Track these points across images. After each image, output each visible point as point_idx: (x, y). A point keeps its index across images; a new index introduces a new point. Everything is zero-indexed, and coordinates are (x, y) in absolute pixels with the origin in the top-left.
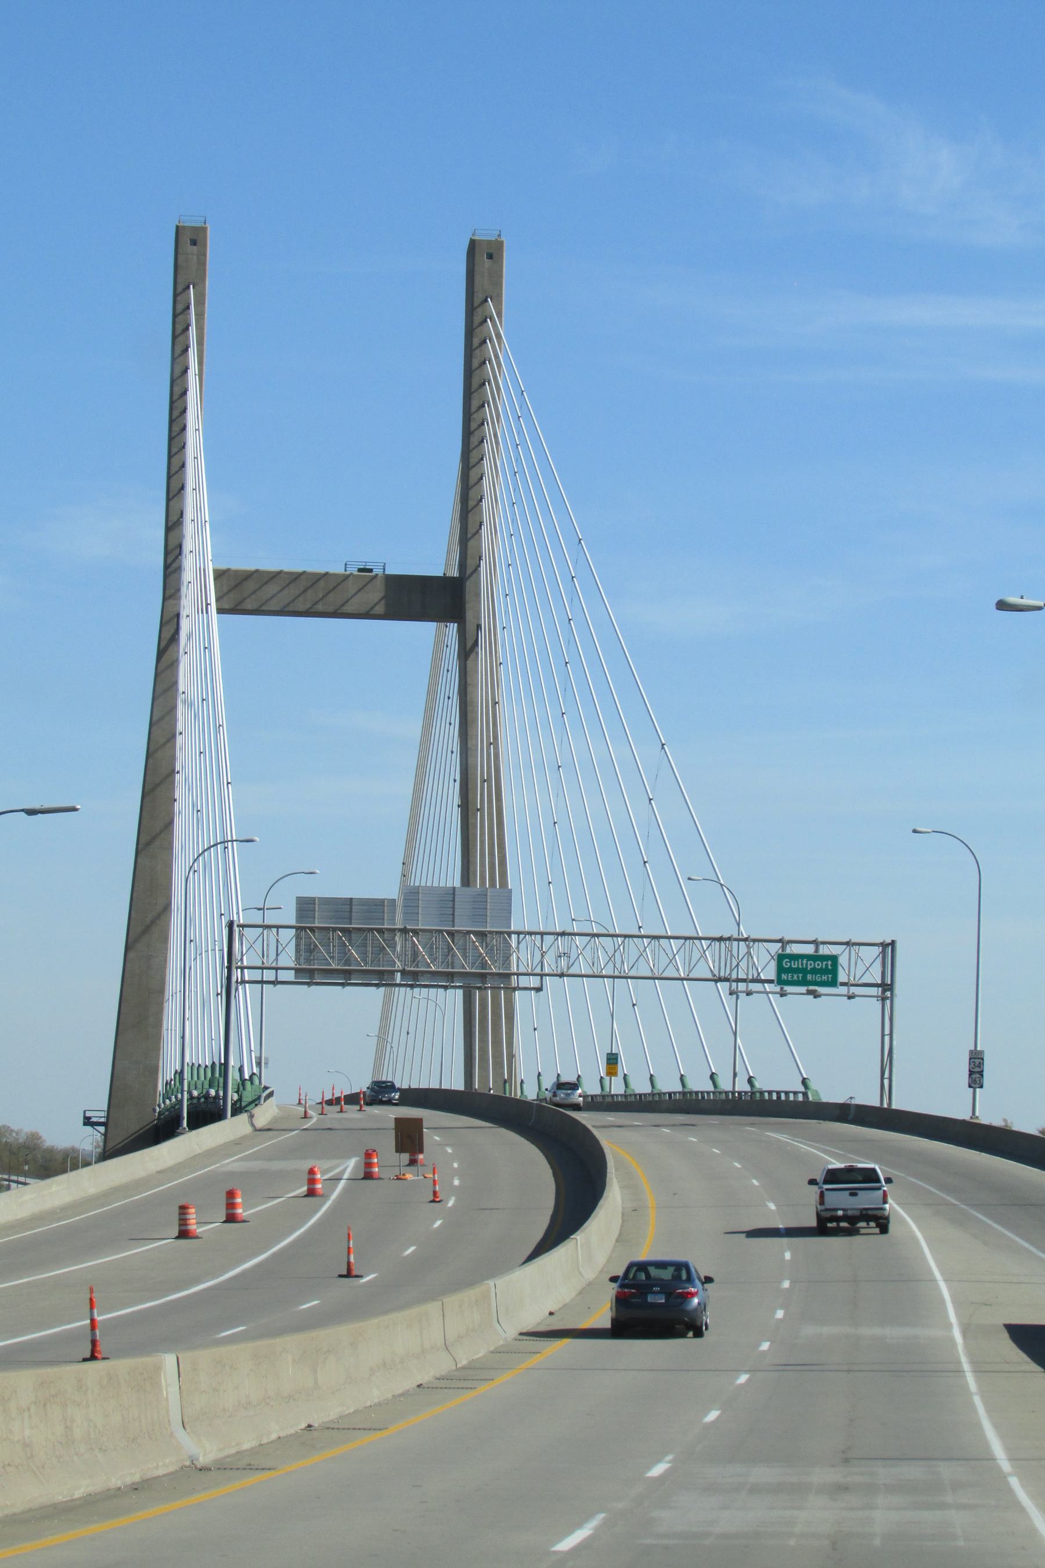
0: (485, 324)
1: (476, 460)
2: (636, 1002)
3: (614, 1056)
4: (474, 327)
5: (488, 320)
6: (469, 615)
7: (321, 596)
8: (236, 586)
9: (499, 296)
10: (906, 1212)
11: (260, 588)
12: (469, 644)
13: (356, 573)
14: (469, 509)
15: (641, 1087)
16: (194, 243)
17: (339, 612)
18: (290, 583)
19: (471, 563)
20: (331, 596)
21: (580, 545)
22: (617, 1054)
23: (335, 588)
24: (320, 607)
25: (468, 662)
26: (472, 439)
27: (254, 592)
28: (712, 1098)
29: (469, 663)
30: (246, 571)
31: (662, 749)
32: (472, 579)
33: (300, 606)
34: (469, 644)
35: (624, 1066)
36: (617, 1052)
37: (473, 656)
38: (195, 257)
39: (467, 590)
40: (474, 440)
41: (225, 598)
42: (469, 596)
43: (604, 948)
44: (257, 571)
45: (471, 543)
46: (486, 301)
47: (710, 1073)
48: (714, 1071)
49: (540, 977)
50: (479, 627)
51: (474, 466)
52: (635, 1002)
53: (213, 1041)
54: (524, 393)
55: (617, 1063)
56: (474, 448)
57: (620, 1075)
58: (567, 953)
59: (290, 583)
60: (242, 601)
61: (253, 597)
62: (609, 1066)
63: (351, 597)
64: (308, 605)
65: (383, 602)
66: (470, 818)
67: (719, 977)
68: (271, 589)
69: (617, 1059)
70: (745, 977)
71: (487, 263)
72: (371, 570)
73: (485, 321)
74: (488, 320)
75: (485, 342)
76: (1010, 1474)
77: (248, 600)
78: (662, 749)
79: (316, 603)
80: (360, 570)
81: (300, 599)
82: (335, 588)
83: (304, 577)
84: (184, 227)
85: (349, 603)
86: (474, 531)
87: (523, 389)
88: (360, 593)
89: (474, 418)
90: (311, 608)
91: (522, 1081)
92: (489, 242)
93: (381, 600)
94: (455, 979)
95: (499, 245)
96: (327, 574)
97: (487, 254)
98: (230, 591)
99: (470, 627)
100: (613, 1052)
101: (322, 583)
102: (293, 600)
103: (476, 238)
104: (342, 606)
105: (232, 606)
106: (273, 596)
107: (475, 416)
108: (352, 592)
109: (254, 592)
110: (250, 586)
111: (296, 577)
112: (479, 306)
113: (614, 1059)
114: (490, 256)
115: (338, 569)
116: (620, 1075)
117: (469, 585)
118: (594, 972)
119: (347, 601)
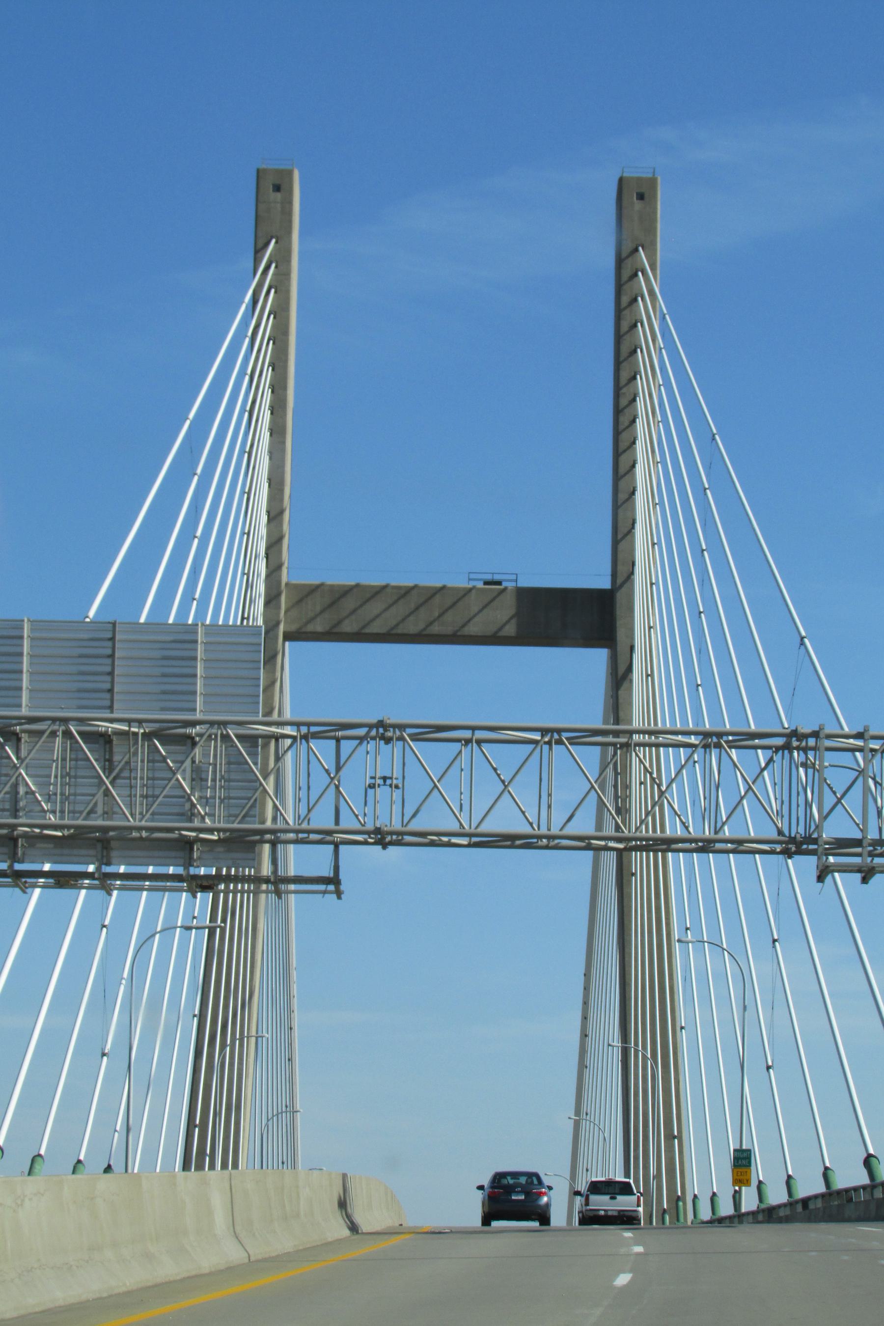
0: (635, 279)
1: (627, 444)
2: (773, 1062)
3: (745, 1155)
4: (622, 283)
5: (640, 274)
6: (621, 634)
7: (437, 614)
8: (332, 604)
9: (653, 243)
10: (237, 740)
11: (361, 606)
12: (622, 670)
13: (480, 585)
14: (619, 504)
15: (777, 1196)
16: (277, 188)
17: (459, 633)
18: (399, 599)
19: (622, 570)
20: (449, 617)
21: (802, 647)
22: (749, 1151)
23: (454, 604)
24: (436, 629)
25: (620, 692)
26: (621, 419)
27: (354, 611)
28: (233, 873)
29: (621, 692)
30: (344, 586)
31: (802, 644)
32: (624, 589)
33: (412, 627)
34: (622, 670)
35: (759, 1169)
36: (749, 1147)
37: (625, 685)
38: (279, 206)
39: (618, 605)
40: (624, 420)
41: (318, 619)
42: (619, 612)
43: (495, 770)
44: (357, 586)
45: (621, 546)
46: (636, 250)
47: (865, 1155)
48: (871, 1151)
49: (332, 847)
50: (632, 648)
51: (625, 451)
52: (770, 1063)
53: (116, 1134)
54: (806, 641)
55: (749, 1165)
56: (624, 430)
57: (754, 1183)
58: (391, 778)
59: (399, 599)
60: (340, 622)
61: (353, 617)
62: (736, 1170)
63: (475, 616)
64: (421, 626)
65: (514, 621)
66: (624, 887)
67: (790, 837)
68: (375, 607)
69: (748, 1158)
70: (858, 835)
71: (638, 205)
72: (499, 583)
73: (636, 275)
74: (640, 274)
75: (635, 300)
76: (808, 846)
77: (346, 622)
78: (802, 644)
79: (431, 623)
80: (486, 583)
81: (411, 618)
82: (454, 604)
83: (414, 592)
84: (265, 170)
85: (472, 622)
86: (626, 530)
87: (803, 634)
88: (485, 611)
89: (624, 394)
90: (425, 629)
91: (695, 1196)
92: (639, 180)
93: (511, 618)
94: (114, 854)
95: (652, 183)
96: (444, 588)
97: (637, 194)
98: (322, 611)
99: (622, 646)
100: (744, 1147)
101: (437, 599)
102: (404, 620)
103: (625, 175)
104: (463, 626)
105: (327, 628)
106: (378, 616)
107: (624, 390)
108: (475, 609)
109: (354, 611)
110: (349, 604)
111: (406, 592)
112: (628, 257)
113: (745, 1158)
114: (641, 197)
115: (460, 582)
116: (754, 1183)
117: (620, 596)
118: (461, 824)
119: (469, 621)
